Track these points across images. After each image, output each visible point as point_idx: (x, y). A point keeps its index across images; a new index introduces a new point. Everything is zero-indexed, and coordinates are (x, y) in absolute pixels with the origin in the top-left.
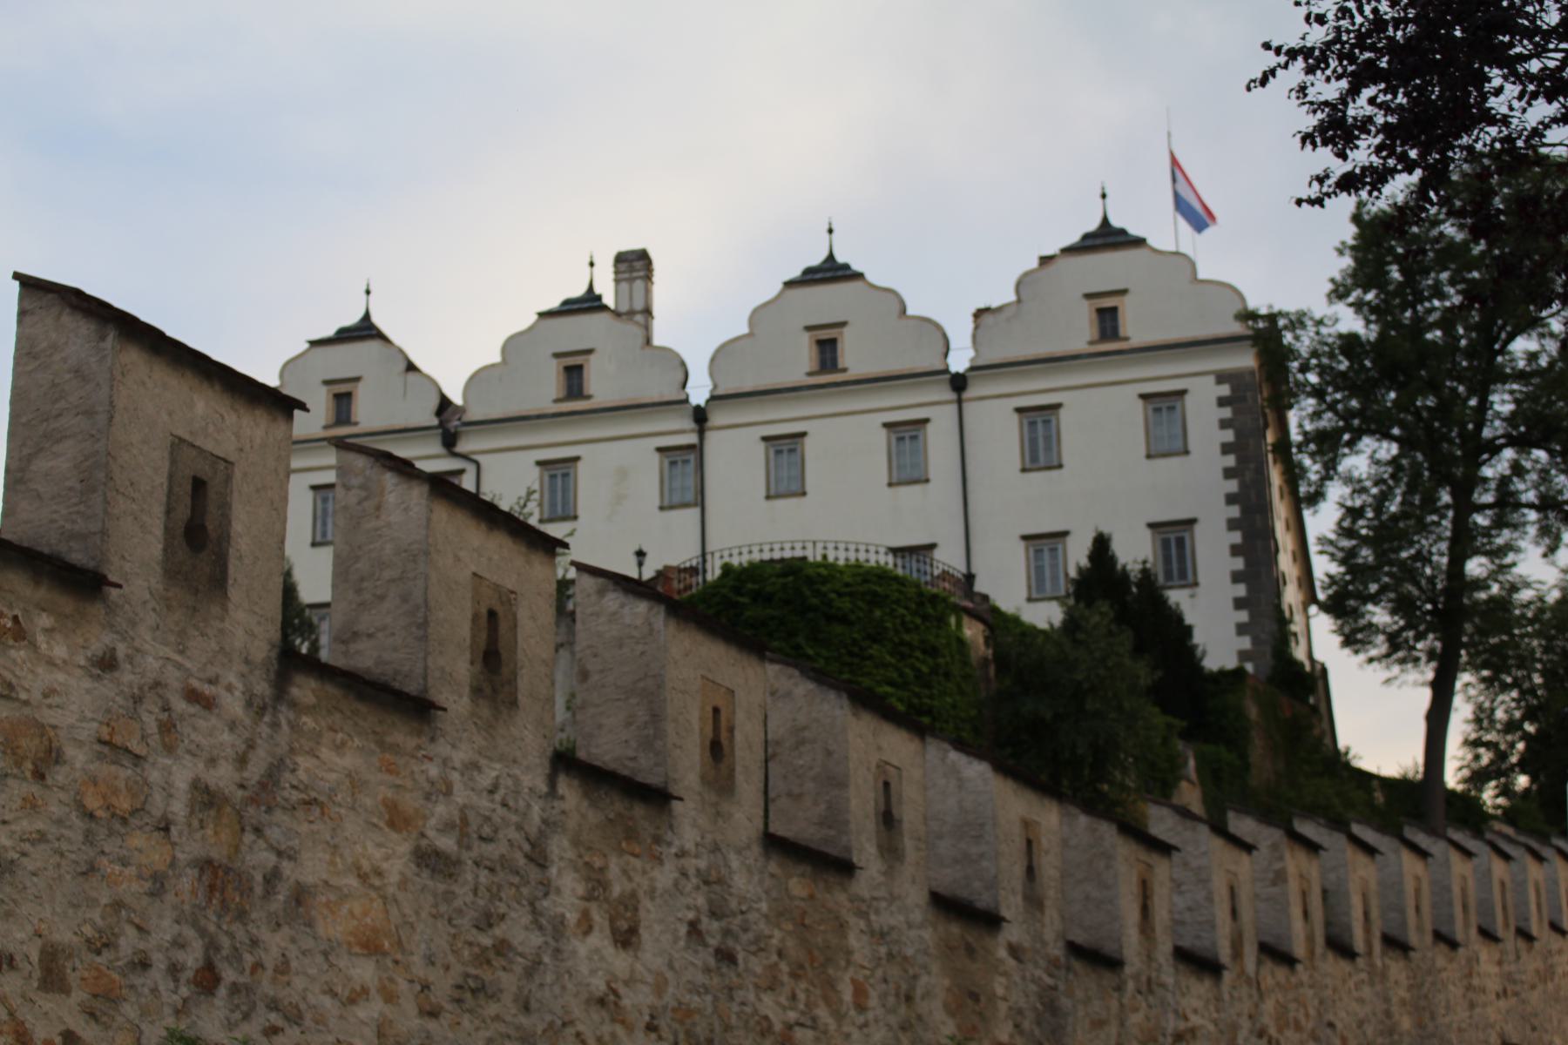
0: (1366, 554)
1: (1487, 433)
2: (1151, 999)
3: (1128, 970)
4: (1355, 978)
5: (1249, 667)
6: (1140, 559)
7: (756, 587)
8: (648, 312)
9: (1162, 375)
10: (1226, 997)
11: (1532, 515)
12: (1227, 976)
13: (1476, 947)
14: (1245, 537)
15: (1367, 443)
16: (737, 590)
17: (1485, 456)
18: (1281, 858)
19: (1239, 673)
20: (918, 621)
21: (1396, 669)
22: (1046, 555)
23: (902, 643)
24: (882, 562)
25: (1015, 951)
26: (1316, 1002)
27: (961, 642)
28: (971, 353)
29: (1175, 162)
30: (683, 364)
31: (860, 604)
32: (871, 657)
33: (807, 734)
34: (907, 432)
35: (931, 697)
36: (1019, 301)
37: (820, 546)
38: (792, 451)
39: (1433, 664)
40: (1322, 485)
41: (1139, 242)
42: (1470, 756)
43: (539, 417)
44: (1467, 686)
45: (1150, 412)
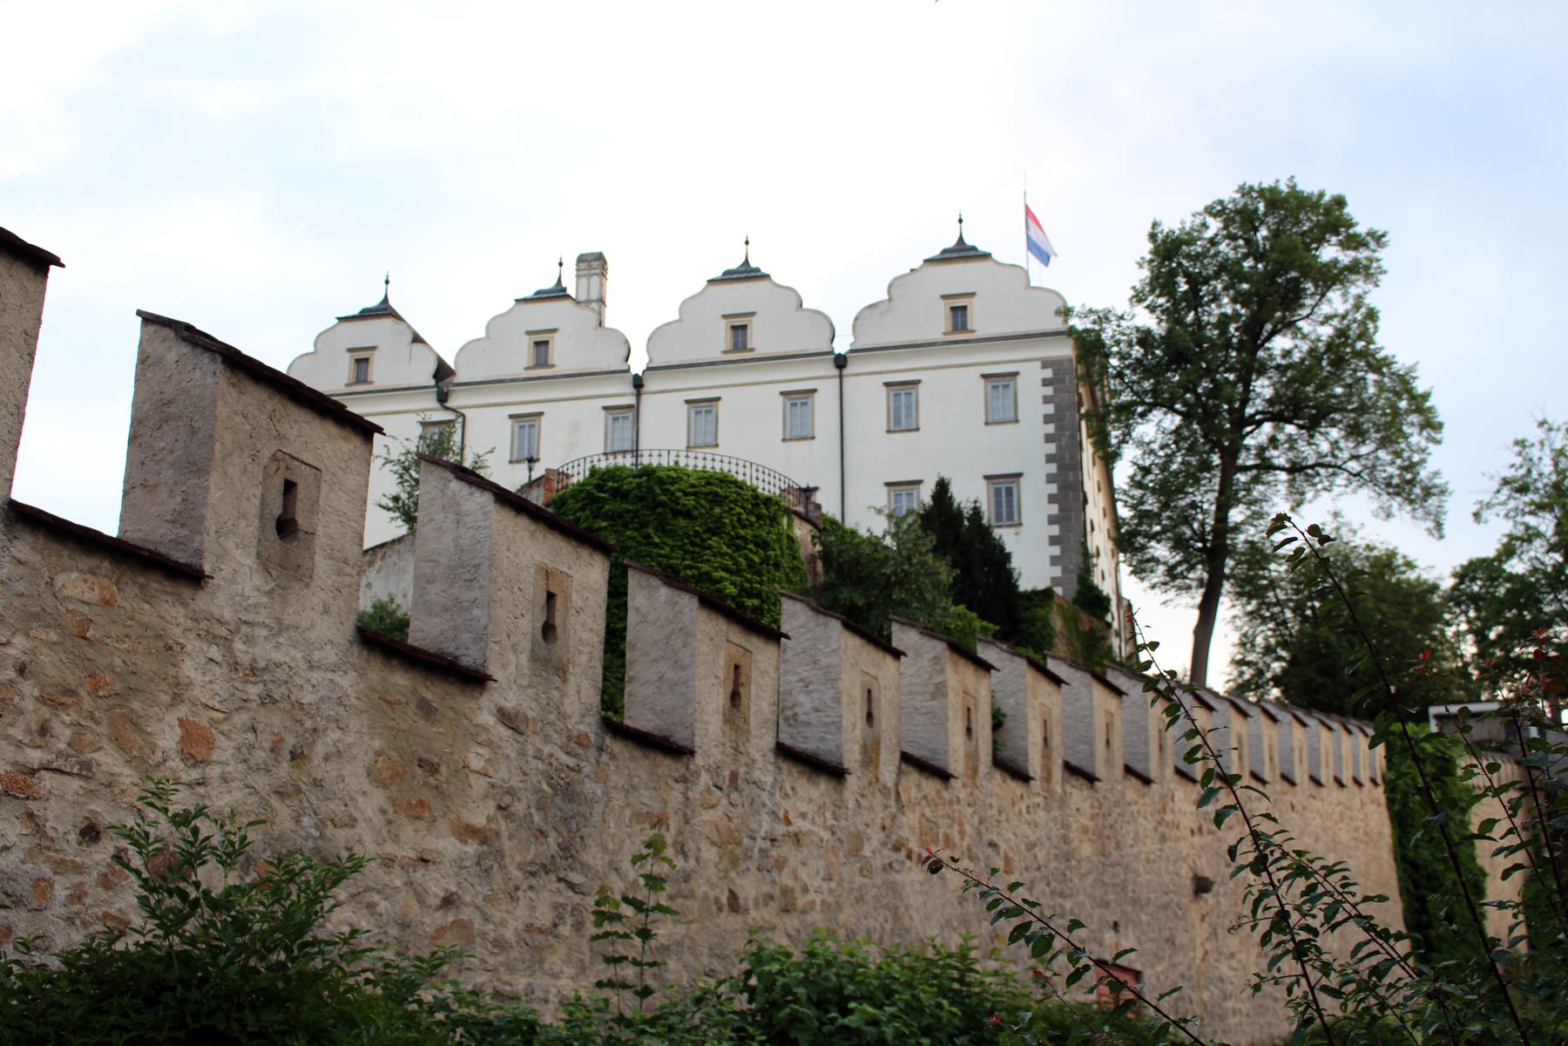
0: (1151, 504)
1: (1249, 411)
2: (735, 796)
3: (699, 760)
4: (1027, 801)
5: (1058, 591)
6: (972, 500)
8: (602, 301)
9: (999, 360)
10: (851, 804)
11: (1283, 476)
12: (852, 782)
13: (1172, 786)
14: (1060, 488)
15: (1157, 414)
16: (600, 488)
17: (1249, 429)
18: (942, 671)
19: (1047, 594)
20: (753, 519)
21: (1172, 594)
22: (904, 497)
23: (738, 537)
24: (726, 470)
25: (507, 718)
26: (976, 821)
27: (791, 539)
30: (627, 342)
31: (703, 502)
32: (710, 547)
33: (173, 409)
34: (799, 398)
35: (761, 583)
37: (673, 454)
38: (708, 412)
39: (1202, 591)
40: (1119, 448)
41: (986, 256)
42: (1235, 673)
43: (513, 380)
44: (1228, 609)
45: (989, 388)
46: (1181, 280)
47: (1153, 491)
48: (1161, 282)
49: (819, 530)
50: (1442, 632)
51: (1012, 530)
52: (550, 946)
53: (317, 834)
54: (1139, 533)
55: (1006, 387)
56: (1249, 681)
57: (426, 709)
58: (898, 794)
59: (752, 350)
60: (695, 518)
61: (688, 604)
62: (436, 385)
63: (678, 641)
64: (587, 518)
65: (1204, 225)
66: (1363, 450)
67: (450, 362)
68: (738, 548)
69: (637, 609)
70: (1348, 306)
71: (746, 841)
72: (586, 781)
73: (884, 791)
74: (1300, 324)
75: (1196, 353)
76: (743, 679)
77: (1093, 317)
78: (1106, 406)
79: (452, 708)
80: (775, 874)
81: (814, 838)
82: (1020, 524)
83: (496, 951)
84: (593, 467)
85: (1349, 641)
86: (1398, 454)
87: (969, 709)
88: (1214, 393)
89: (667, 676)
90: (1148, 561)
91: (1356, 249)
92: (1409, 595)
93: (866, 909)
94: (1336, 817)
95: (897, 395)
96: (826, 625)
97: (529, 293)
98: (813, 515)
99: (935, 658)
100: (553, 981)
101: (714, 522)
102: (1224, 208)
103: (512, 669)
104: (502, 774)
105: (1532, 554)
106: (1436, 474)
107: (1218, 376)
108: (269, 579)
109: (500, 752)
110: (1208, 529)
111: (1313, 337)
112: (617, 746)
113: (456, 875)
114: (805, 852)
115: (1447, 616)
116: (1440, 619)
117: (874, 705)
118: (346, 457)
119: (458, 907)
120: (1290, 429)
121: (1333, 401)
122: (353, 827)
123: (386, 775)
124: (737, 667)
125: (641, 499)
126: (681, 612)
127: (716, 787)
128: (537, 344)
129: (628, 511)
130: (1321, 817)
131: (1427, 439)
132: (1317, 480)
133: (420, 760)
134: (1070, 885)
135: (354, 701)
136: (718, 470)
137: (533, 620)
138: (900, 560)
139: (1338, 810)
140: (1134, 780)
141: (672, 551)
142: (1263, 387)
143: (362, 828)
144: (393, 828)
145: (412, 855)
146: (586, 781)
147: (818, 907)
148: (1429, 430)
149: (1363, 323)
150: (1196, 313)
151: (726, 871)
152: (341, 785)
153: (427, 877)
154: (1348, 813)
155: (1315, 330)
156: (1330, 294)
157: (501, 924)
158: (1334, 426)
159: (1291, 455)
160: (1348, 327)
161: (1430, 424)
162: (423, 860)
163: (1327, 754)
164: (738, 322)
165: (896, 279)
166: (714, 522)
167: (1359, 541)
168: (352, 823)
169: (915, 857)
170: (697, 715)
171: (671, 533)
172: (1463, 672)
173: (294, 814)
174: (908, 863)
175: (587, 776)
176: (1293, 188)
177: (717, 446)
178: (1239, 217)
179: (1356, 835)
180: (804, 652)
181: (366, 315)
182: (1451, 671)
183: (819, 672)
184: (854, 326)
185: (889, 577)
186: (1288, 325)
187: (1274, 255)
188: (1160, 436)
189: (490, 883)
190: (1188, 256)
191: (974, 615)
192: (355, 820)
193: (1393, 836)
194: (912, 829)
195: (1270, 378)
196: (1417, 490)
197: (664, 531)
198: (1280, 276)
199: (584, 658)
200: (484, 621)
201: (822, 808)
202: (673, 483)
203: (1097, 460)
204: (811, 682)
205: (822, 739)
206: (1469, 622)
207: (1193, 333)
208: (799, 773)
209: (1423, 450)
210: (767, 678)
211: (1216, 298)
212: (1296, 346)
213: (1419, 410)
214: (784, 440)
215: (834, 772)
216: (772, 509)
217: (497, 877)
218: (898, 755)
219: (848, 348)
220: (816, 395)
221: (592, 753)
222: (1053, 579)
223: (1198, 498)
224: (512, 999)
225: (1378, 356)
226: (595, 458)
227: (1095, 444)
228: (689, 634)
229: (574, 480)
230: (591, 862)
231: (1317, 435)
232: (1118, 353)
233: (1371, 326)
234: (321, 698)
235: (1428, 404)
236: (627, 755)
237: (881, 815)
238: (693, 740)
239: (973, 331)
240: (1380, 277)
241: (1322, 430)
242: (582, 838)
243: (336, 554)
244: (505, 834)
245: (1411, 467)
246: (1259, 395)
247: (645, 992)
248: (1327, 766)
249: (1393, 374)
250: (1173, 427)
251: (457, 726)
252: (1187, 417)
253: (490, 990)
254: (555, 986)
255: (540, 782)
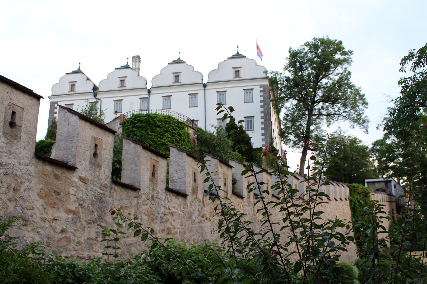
0: (289, 124)
1: (316, 99)
2: (153, 202)
3: (142, 192)
4: (242, 204)
5: (264, 148)
7: (139, 119)
8: (139, 69)
9: (248, 85)
10: (189, 204)
11: (325, 117)
12: (189, 198)
14: (264, 120)
15: (291, 100)
16: (135, 119)
17: (316, 104)
18: (217, 168)
19: (261, 149)
20: (177, 128)
23: (173, 133)
24: (170, 115)
25: (82, 179)
27: (188, 133)
28: (208, 79)
29: (257, 45)
30: (146, 80)
31: (163, 123)
32: (165, 136)
34: (193, 96)
36: (218, 68)
37: (155, 110)
39: (303, 148)
41: (245, 57)
43: (114, 91)
45: (245, 93)
46: (297, 63)
47: (290, 121)
48: (292, 64)
49: (196, 131)
50: (369, 159)
51: (252, 132)
52: (95, 244)
53: (21, 212)
54: (286, 133)
55: (250, 92)
56: (316, 173)
57: (57, 177)
58: (203, 202)
59: (180, 82)
60: (161, 128)
61: (139, 148)
62: (93, 92)
63: (136, 158)
64: (131, 128)
65: (304, 49)
66: (347, 110)
67: (97, 85)
68: (173, 136)
69: (125, 150)
70: (343, 71)
71: (156, 215)
72: (107, 197)
73: (199, 201)
74: (330, 76)
75: (301, 83)
76: (156, 169)
77: (273, 74)
78: (277, 98)
79: (65, 177)
80: (165, 224)
81: (177, 214)
82: (254, 130)
83: (78, 245)
84: (133, 114)
85: (343, 162)
86: (356, 111)
87: (225, 178)
88: (306, 94)
89: (133, 168)
90: (288, 140)
91: (345, 55)
92: (360, 149)
93: (193, 233)
94: (335, 209)
95: (220, 95)
96: (182, 155)
97: (119, 67)
98: (194, 127)
99: (215, 164)
100: (96, 254)
101: (166, 129)
102: (309, 44)
103: (84, 165)
104: (80, 195)
105: (392, 138)
106: (366, 116)
107: (308, 90)
108: (7, 139)
109: (80, 189)
110: (304, 131)
111: (333, 79)
112: (116, 188)
113: (65, 223)
114: (175, 217)
115: (370, 155)
116: (368, 156)
117: (196, 177)
118: (31, 105)
119: (66, 233)
120: (327, 104)
121: (339, 96)
122: (33, 210)
123: (44, 195)
124: (154, 166)
125: (146, 122)
126: (137, 150)
127: (147, 199)
128: (121, 81)
129: (143, 126)
130: (330, 209)
131: (364, 107)
132: (334, 118)
133: (54, 191)
134: (255, 227)
135: (34, 174)
136: (168, 115)
137: (90, 152)
138: (218, 139)
139: (335, 207)
140: (275, 198)
141: (155, 137)
142: (320, 93)
143: (36, 210)
144: (46, 210)
145: (52, 218)
146: (107, 197)
147: (178, 233)
148: (364, 105)
149: (347, 76)
150: (302, 73)
151: (150, 223)
152: (29, 198)
153: (56, 224)
154: (338, 208)
155: (334, 77)
156: (338, 68)
157: (80, 237)
158: (339, 103)
159: (327, 111)
160: (343, 76)
161: (365, 103)
162: (55, 219)
163: (332, 192)
164: (177, 75)
165: (220, 63)
166: (166, 129)
167: (346, 135)
168: (33, 209)
169: (208, 219)
170: (141, 179)
171: (155, 132)
172: (375, 170)
173: (14, 206)
174: (206, 221)
175: (107, 196)
176: (328, 38)
177: (171, 108)
178: (314, 47)
179: (340, 214)
180: (176, 162)
181: (74, 72)
182: (371, 170)
183: (180, 168)
184: (208, 76)
185: (215, 144)
186: (326, 76)
187: (322, 57)
188: (292, 106)
189: (76, 226)
190: (299, 57)
191: (240, 155)
192: (34, 208)
193: (351, 214)
194: (208, 212)
195: (321, 90)
196: (361, 121)
197: (152, 131)
198: (325, 63)
199: (106, 163)
200: (75, 152)
201: (180, 205)
202: (155, 118)
203: (275, 113)
204: (178, 170)
205: (181, 186)
206: (376, 157)
207: (301, 78)
208: (173, 195)
209: (363, 110)
210: (163, 169)
211: (307, 69)
212: (329, 82)
213: (362, 99)
214: (189, 107)
215: (184, 196)
216: (183, 125)
217: (79, 224)
218: (203, 191)
219: (207, 82)
220: (198, 95)
221: (109, 190)
222: (263, 145)
223: (302, 123)
224: (83, 258)
225: (351, 84)
226: (134, 111)
227: (274, 108)
228: (139, 157)
229: (128, 117)
230: (108, 220)
231: (334, 106)
232: (281, 83)
233: (349, 76)
234: (23, 173)
235: (364, 98)
236: (119, 190)
237: (198, 207)
238: (140, 186)
239: (241, 77)
240: (351, 63)
241: (336, 104)
242: (105, 213)
243: (28, 132)
244: (81, 212)
245: (359, 115)
246: (318, 95)
247: (116, 256)
248: (332, 195)
249: (355, 89)
250: (295, 104)
251: (66, 181)
252: (299, 101)
253: (76, 256)
254: (96, 255)
255: (92, 198)
